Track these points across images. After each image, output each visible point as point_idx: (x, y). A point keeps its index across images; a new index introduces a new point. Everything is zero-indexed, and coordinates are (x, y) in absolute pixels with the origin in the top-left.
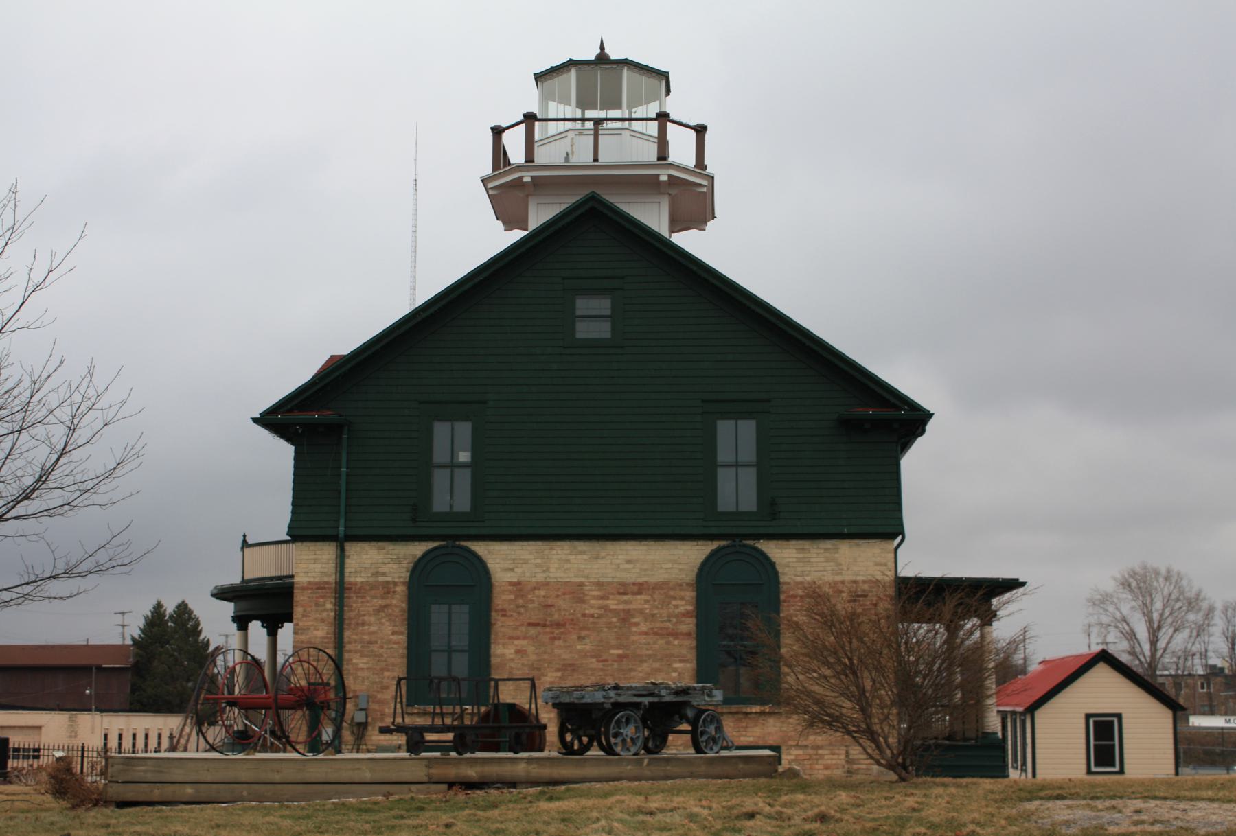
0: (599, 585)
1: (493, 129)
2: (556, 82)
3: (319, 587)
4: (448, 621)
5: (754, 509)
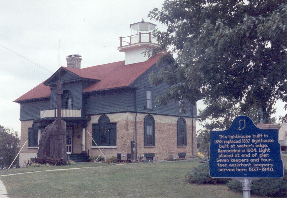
0: (167, 124)
1: (120, 37)
2: (135, 26)
3: (131, 122)
4: (149, 130)
5: (62, 116)
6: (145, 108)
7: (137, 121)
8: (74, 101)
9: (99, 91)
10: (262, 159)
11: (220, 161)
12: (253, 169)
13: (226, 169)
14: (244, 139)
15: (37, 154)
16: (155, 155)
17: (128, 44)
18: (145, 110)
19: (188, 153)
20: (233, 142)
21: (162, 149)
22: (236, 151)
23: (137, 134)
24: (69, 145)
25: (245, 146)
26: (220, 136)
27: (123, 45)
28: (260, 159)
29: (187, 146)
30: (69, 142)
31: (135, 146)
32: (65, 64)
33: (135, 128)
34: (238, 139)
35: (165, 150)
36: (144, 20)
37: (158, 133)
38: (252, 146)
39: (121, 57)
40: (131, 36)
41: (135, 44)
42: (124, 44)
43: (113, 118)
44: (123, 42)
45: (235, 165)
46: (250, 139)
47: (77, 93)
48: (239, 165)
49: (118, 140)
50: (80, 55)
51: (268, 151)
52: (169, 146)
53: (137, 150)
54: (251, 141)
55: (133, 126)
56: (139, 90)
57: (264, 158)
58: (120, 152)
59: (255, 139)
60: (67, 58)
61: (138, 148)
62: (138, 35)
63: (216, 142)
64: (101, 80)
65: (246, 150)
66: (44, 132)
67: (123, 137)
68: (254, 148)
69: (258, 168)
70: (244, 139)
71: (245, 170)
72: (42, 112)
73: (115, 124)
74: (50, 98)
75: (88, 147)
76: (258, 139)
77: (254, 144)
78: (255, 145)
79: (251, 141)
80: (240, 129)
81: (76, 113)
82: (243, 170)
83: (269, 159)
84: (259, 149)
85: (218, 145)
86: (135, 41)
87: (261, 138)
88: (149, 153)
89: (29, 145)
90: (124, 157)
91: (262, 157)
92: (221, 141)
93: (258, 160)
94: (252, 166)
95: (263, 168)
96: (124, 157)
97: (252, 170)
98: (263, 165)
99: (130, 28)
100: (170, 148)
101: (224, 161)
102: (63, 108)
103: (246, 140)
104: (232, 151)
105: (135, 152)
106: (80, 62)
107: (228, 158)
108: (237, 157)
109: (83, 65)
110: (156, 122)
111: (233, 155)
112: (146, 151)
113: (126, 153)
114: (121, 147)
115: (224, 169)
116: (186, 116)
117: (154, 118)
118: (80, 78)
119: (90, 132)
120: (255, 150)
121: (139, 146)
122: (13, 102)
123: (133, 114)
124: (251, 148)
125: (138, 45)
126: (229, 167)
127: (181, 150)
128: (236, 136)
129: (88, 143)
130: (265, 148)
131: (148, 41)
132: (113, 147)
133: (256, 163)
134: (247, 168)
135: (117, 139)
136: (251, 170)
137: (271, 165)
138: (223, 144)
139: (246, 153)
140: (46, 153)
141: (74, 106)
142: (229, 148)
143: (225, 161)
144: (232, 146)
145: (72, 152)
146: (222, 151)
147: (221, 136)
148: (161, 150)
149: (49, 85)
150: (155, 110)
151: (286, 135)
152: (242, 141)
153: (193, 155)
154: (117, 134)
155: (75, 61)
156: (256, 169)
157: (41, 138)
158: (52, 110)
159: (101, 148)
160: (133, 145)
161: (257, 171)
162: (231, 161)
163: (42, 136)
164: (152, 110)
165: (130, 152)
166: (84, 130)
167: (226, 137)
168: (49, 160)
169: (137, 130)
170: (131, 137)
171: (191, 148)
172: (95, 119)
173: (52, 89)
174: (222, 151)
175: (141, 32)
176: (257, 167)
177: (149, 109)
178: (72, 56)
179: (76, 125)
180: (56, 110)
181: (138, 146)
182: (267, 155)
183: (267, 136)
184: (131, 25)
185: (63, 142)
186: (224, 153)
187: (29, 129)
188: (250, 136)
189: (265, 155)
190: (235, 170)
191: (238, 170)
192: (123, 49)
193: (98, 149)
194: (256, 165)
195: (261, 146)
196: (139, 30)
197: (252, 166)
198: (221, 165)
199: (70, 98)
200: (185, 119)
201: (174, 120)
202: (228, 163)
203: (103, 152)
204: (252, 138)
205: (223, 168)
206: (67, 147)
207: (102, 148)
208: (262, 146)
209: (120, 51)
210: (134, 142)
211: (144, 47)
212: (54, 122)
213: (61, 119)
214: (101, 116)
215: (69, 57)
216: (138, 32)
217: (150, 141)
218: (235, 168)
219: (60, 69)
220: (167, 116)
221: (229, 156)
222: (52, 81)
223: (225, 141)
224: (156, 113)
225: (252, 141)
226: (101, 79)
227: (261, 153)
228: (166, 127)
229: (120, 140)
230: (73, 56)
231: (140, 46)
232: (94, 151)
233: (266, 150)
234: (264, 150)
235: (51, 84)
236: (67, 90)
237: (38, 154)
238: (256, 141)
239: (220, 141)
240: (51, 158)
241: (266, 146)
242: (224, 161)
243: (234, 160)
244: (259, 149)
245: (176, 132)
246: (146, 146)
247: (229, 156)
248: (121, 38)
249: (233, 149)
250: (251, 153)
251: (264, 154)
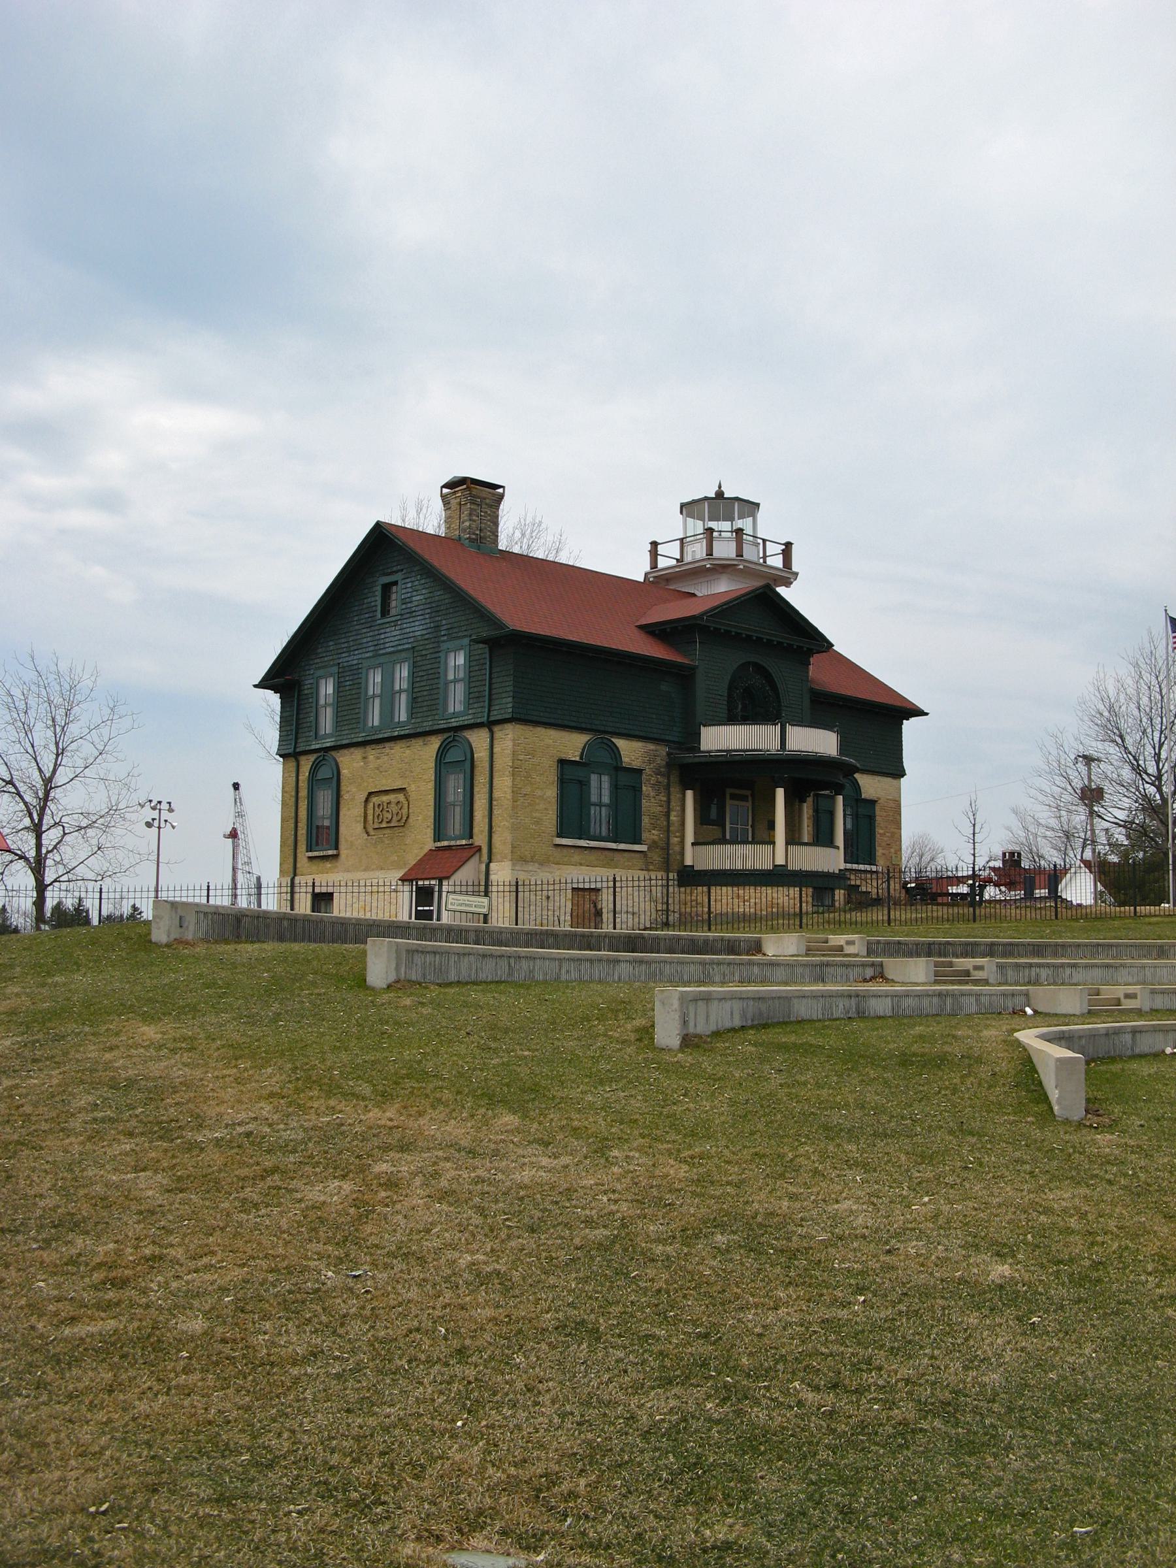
17: (674, 562)
40: (682, 540)
42: (663, 563)
73: (872, 803)
86: (697, 551)
122: (255, 686)
131: (733, 555)
175: (713, 524)
184: (682, 506)
248: (655, 544)
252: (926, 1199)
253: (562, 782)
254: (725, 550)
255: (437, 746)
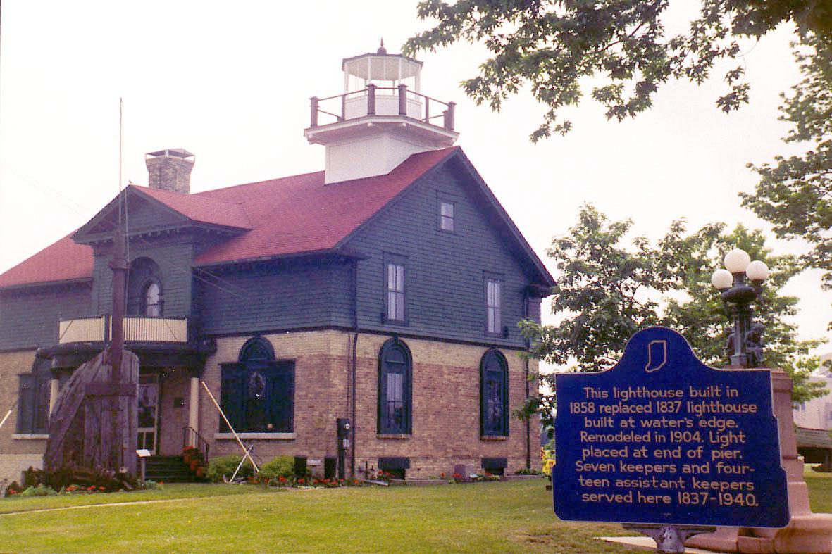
3: (341, 358)
4: (394, 382)
6: (383, 317)
7: (357, 356)
8: (165, 292)
9: (243, 264)
10: (719, 466)
11: (587, 467)
12: (692, 497)
13: (607, 496)
14: (660, 399)
15: (42, 455)
16: (413, 465)
17: (336, 120)
18: (383, 322)
19: (513, 458)
20: (629, 409)
21: (434, 445)
22: (637, 438)
23: (357, 397)
24: (145, 430)
25: (667, 423)
26: (587, 389)
27: (320, 123)
28: (713, 465)
29: (511, 437)
30: (145, 420)
31: (351, 433)
32: (141, 179)
33: (351, 377)
34: (644, 401)
35: (444, 448)
36: (384, 46)
37: (422, 396)
38: (687, 422)
39: (313, 160)
40: (344, 96)
41: (358, 119)
42: (323, 120)
43: (285, 346)
44: (319, 113)
45: (634, 483)
46: (680, 402)
47: (177, 265)
48: (646, 484)
49: (298, 416)
50: (189, 150)
51: (739, 438)
52: (454, 438)
53: (358, 447)
54: (684, 407)
55: (345, 371)
56: (365, 263)
57: (727, 462)
58: (305, 453)
59: (697, 401)
60: (147, 161)
61: (358, 442)
62: (367, 92)
63: (576, 407)
64: (250, 230)
65: (668, 436)
66: (66, 387)
67: (315, 407)
68: (692, 431)
69: (706, 494)
70: (660, 399)
71: (666, 499)
72: (63, 325)
73: (290, 364)
74: (91, 282)
75: (205, 436)
76: (707, 400)
77: (692, 416)
78: (696, 421)
79: (684, 407)
80: (649, 369)
81: (172, 331)
82: (660, 500)
83: (743, 467)
84: (711, 433)
85: (579, 418)
86: (358, 110)
87: (715, 399)
88: (393, 455)
89: (21, 428)
90: (315, 463)
91: (720, 459)
92: (592, 405)
93: (705, 469)
94: (689, 488)
95: (723, 493)
96: (315, 463)
97: (686, 500)
98: (722, 483)
99: (341, 70)
100: (458, 443)
101: (598, 470)
102: (130, 314)
103: (670, 405)
104: (624, 438)
105: (349, 453)
106: (189, 173)
107: (610, 460)
108: (640, 456)
109: (199, 182)
110: (415, 360)
111: (626, 451)
112: (384, 450)
113: (324, 454)
114: (307, 437)
115: (600, 496)
116: (506, 344)
117: (411, 350)
118: (185, 222)
119: (214, 388)
120: (697, 437)
121: (364, 433)
123: (347, 335)
124: (683, 428)
125: (367, 124)
126: (613, 490)
127: (493, 451)
128: (638, 391)
129: (207, 421)
130: (730, 432)
132: (283, 438)
133: (701, 477)
134: (673, 492)
135: (296, 413)
136: (684, 498)
137: (750, 486)
138: (596, 416)
139: (670, 445)
140: (71, 452)
141: (165, 308)
142: (615, 431)
143: (602, 467)
144: (624, 424)
145: (154, 452)
146: (592, 438)
147: (590, 391)
148: (431, 447)
149: (91, 243)
150: (413, 324)
151: (830, 416)
152: (654, 407)
153: (528, 466)
154: (296, 395)
155: (174, 168)
156: (701, 498)
157: (59, 404)
158: (98, 320)
159: (243, 440)
160: (343, 430)
161: (704, 503)
162: (622, 468)
163: (60, 400)
164: (406, 323)
165: (334, 454)
166: (195, 381)
167: (605, 394)
168: (81, 475)
169: (358, 386)
170: (337, 407)
171: (520, 444)
172: (230, 349)
173: (97, 255)
174: (592, 438)
175: (375, 82)
176: (704, 490)
177: (395, 322)
178: (162, 153)
179: (168, 367)
180: (109, 317)
181: (358, 435)
182: (735, 452)
183: (734, 393)
184: (345, 61)
185: (126, 417)
186: (598, 445)
187: (23, 376)
188: (679, 393)
189: (727, 454)
190: (635, 496)
191: (642, 499)
192: (318, 135)
193: (235, 440)
194: (699, 485)
195: (715, 422)
196: (369, 76)
197: (689, 488)
198: (588, 482)
199: (155, 283)
200: (506, 355)
201: (470, 357)
202: (610, 476)
203: (251, 452)
204: (686, 397)
205: (594, 490)
206: (141, 435)
207: (250, 440)
208: (721, 424)
209: (312, 141)
210: (347, 421)
211: (384, 132)
212: (100, 355)
213: (127, 349)
214: (250, 340)
215: (154, 157)
216: (368, 84)
217: (396, 420)
218: (635, 491)
219: (123, 193)
220: (450, 345)
221: (613, 453)
222: (99, 231)
223: (601, 407)
224: (415, 333)
225: (686, 406)
226: (249, 227)
227: (717, 447)
228: (445, 376)
229: (306, 415)
230: (167, 155)
231: (371, 127)
232: (224, 449)
233: (733, 439)
234: (726, 437)
235: (96, 240)
236: (149, 259)
237: (47, 459)
238: (701, 409)
239: (587, 406)
240: (88, 470)
241: (730, 423)
242: (598, 470)
243: (630, 468)
244: (711, 433)
245: (477, 393)
246: (384, 436)
247: (613, 453)
248: (315, 101)
249: (627, 431)
250: (685, 446)
251: (725, 449)
252: (528, 519)
253: (411, 429)
254: (387, 107)
255: (243, 343)
